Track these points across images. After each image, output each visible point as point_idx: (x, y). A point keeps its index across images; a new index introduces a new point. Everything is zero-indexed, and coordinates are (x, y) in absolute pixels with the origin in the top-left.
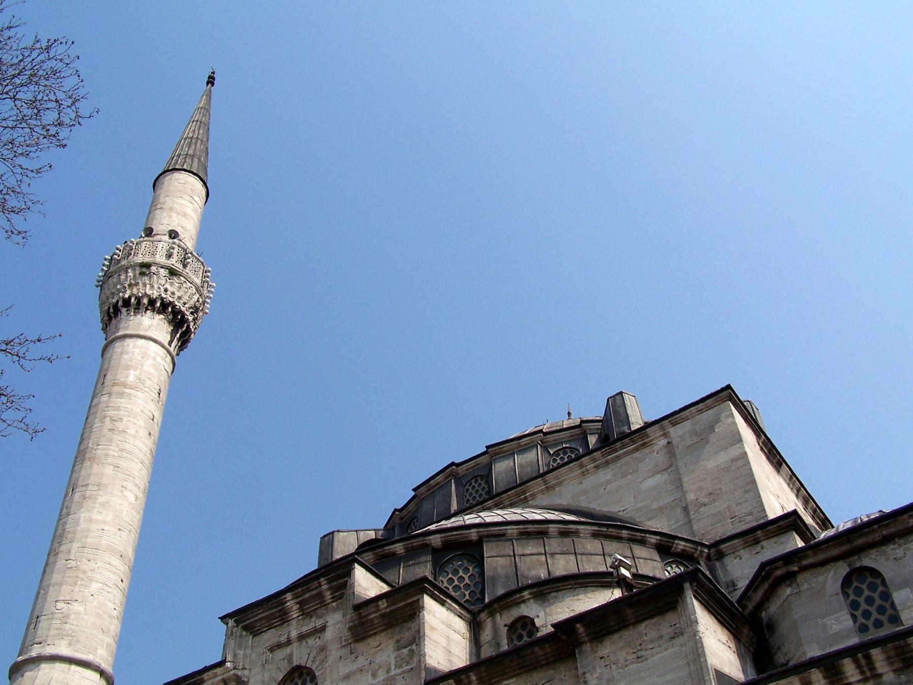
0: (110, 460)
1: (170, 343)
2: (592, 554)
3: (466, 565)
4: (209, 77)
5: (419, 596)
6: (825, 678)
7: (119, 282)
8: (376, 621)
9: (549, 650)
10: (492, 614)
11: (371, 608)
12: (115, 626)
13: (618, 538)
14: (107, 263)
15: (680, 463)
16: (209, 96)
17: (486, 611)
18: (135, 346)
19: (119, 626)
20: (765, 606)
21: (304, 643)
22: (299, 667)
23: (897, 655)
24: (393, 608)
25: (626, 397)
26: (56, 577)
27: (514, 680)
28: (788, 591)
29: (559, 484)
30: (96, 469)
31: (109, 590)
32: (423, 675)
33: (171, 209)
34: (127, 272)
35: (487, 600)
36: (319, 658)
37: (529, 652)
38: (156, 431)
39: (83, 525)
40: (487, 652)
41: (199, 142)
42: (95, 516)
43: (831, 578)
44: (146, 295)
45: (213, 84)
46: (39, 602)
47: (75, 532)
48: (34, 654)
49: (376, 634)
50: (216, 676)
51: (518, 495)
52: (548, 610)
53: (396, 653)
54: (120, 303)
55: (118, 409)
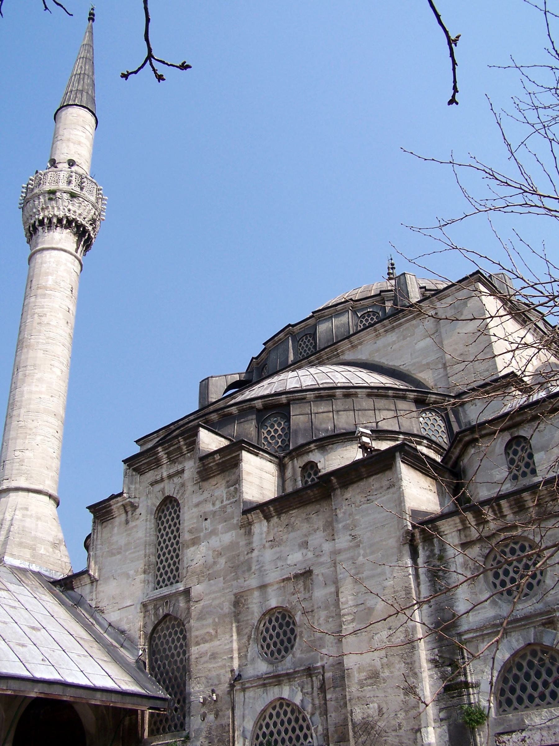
0: (40, 346)
1: (76, 251)
2: (366, 410)
3: (279, 421)
4: (90, 14)
5: (239, 452)
6: (473, 517)
7: (34, 206)
8: (214, 468)
9: (316, 492)
10: (292, 459)
11: (210, 459)
12: (56, 464)
13: (386, 397)
14: (24, 195)
15: (443, 330)
16: (91, 33)
17: (288, 457)
18: (50, 257)
19: (59, 463)
20: (462, 458)
21: (172, 480)
22: (169, 497)
23: (515, 504)
24: (224, 459)
25: (408, 276)
26: (12, 434)
27: (296, 510)
28: (473, 451)
29: (360, 344)
30: (31, 354)
31: (49, 440)
32: (242, 506)
33: (69, 140)
34: (39, 198)
35: (291, 448)
36: (181, 492)
37: (304, 493)
38: (72, 320)
39: (26, 396)
40: (289, 489)
41: (86, 77)
42: (34, 389)
43: (499, 443)
44: (55, 215)
45: (93, 20)
46: (4, 451)
47: (21, 401)
48: (4, 487)
49: (214, 476)
50: (118, 502)
51: (332, 351)
52: (326, 457)
53: (226, 490)
54: (37, 223)
55: (43, 307)
